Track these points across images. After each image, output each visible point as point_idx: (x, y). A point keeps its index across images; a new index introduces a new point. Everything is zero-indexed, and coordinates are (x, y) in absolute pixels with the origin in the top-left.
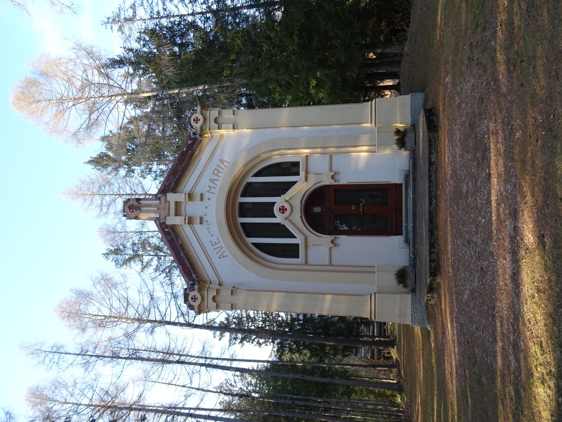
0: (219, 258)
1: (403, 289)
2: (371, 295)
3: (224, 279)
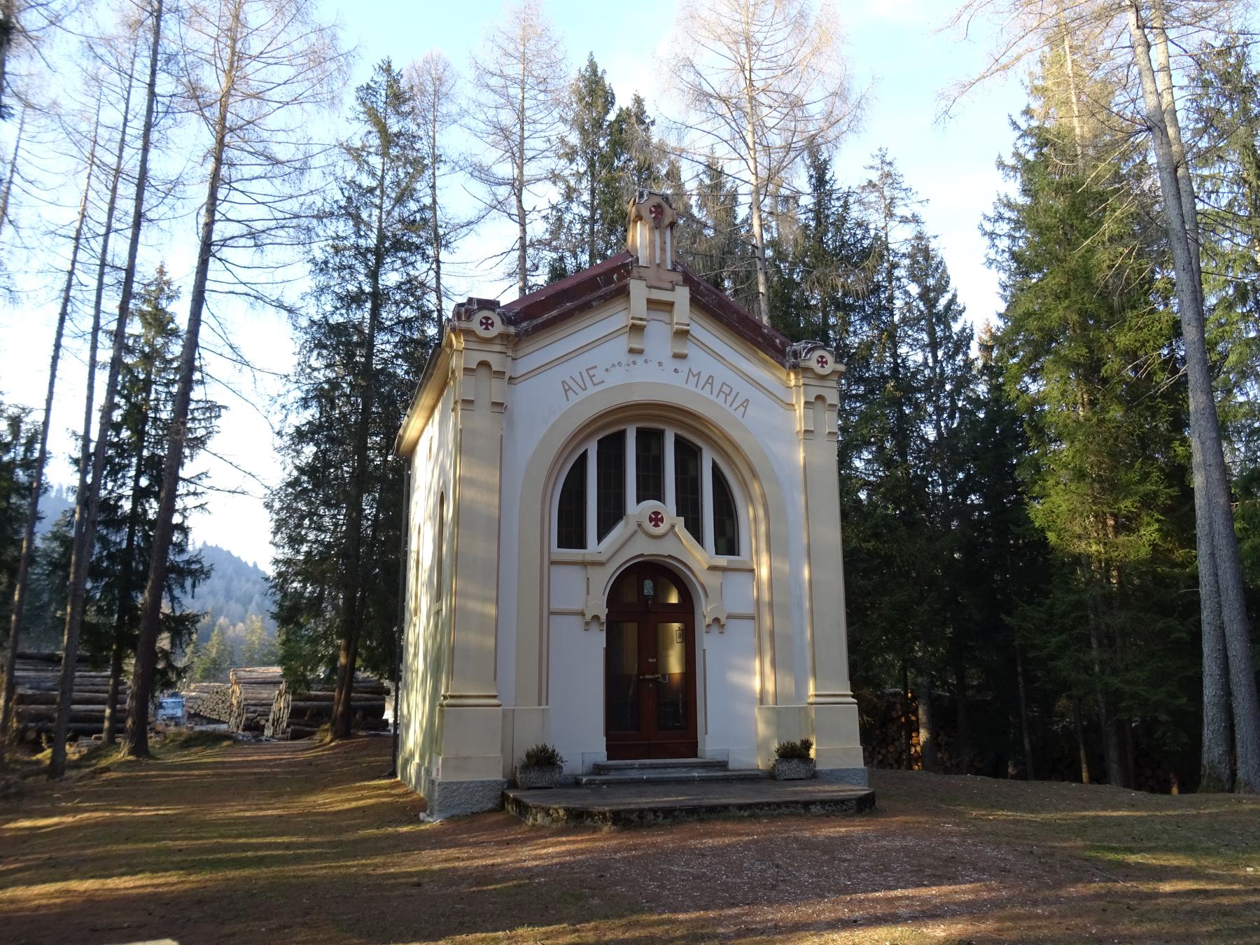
1: (517, 763)
3: (521, 388)
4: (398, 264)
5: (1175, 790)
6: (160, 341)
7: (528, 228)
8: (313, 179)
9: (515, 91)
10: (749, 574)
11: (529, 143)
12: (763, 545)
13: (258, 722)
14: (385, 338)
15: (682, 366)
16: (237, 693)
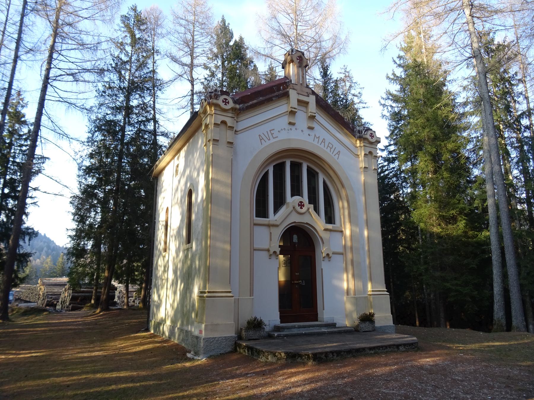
0: (259, 135)
3: (240, 136)
4: (137, 96)
5: (448, 327)
6: (17, 126)
7: (195, 86)
8: (100, 54)
9: (191, 27)
10: (341, 233)
11: (196, 50)
12: (347, 220)
13: (53, 303)
14: (130, 129)
15: (312, 133)
16: (42, 289)
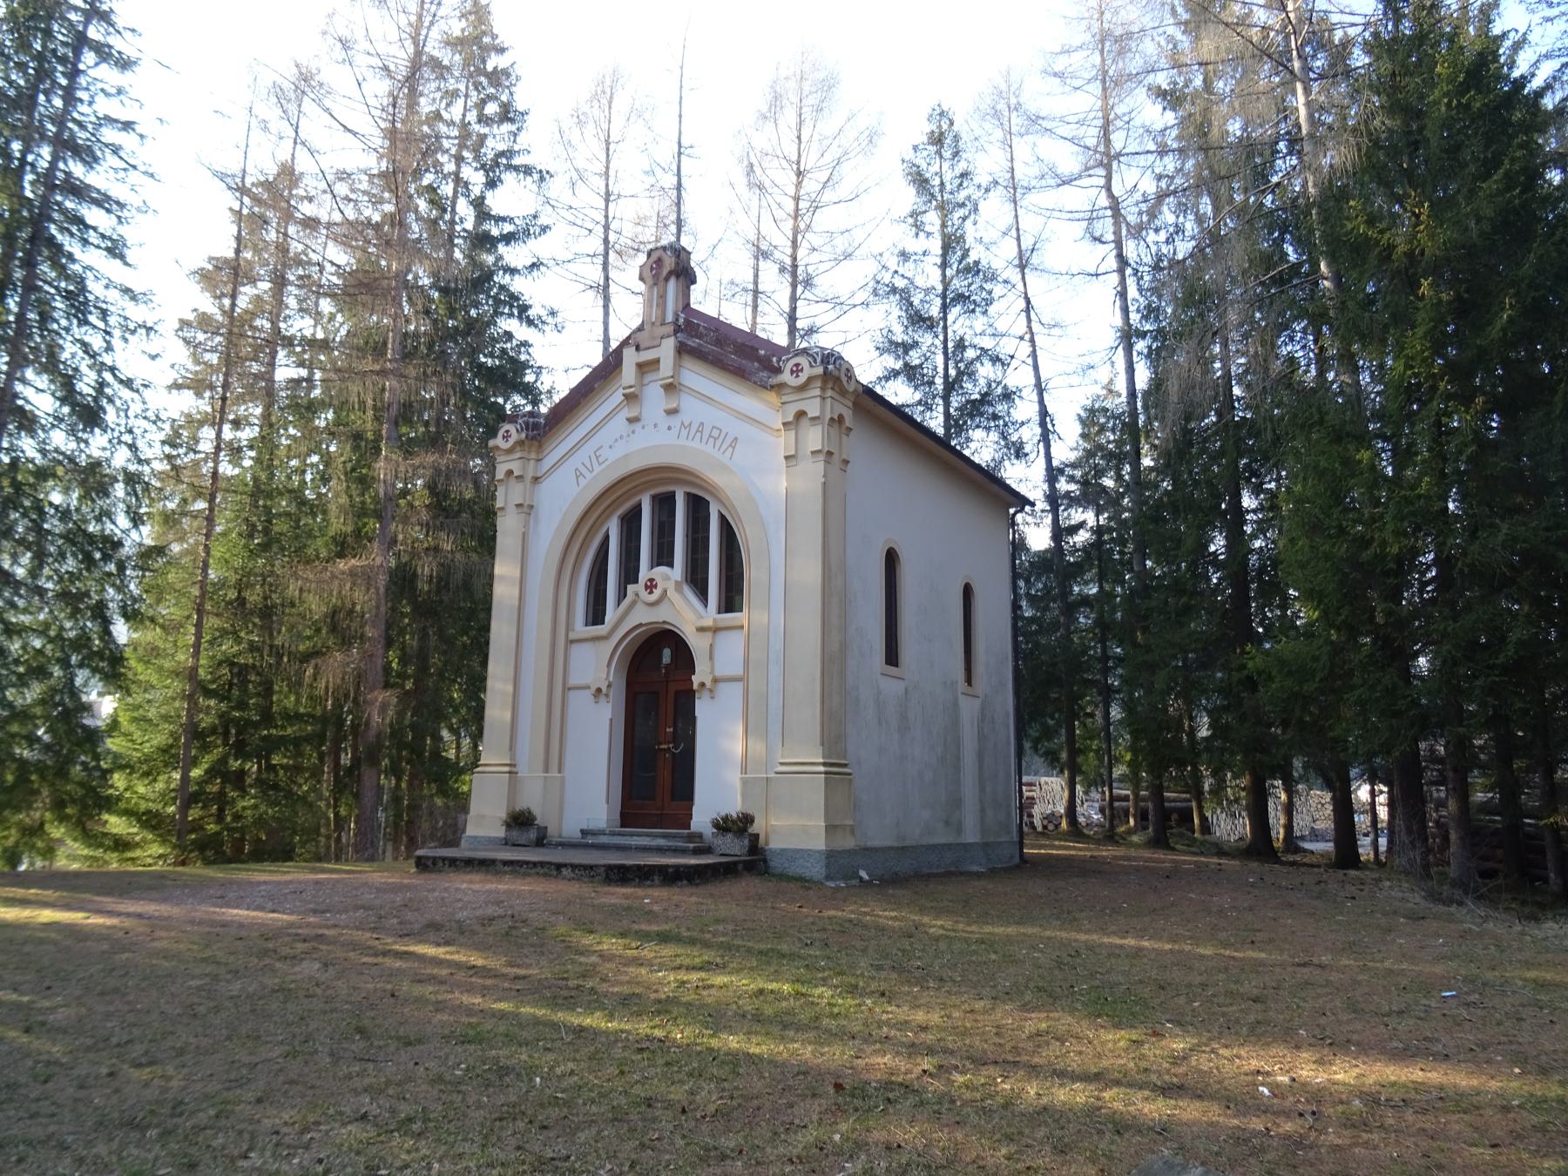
2: (510, 765)
3: (545, 485)
15: (675, 421)
